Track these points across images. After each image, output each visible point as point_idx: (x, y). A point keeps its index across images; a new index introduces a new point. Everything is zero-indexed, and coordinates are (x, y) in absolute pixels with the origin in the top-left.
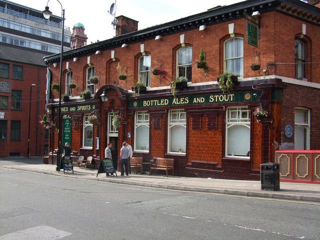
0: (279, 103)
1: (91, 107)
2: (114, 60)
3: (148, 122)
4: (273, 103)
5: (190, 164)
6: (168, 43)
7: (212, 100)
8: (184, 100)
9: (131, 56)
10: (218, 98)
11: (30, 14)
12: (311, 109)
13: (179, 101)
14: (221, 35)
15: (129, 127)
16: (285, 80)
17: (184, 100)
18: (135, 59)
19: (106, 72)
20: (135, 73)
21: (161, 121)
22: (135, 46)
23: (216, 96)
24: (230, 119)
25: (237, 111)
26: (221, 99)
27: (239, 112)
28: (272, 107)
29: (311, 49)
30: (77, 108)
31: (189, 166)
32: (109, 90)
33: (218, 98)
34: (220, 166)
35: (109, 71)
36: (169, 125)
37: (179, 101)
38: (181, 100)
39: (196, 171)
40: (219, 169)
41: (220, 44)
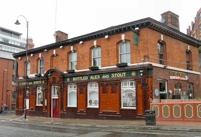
0: (151, 77)
1: (42, 82)
2: (55, 55)
3: (75, 90)
4: (148, 77)
5: (79, 111)
6: (87, 46)
7: (113, 76)
8: (97, 77)
9: (65, 52)
10: (117, 75)
11: (2, 31)
12: (167, 80)
13: (94, 77)
14: (118, 41)
15: (65, 92)
16: (154, 64)
17: (97, 77)
18: (68, 55)
19: (51, 62)
20: (67, 62)
21: (84, 89)
22: (50, 51)
23: (116, 74)
24: (70, 89)
25: (128, 82)
26: (119, 76)
27: (129, 83)
28: (147, 79)
29: (166, 48)
30: (33, 83)
31: (101, 114)
32: (52, 71)
33: (117, 75)
34: (118, 113)
35: (52, 61)
36: (88, 91)
37: (94, 77)
38: (95, 77)
39: (105, 116)
40: (117, 115)
41: (117, 45)
